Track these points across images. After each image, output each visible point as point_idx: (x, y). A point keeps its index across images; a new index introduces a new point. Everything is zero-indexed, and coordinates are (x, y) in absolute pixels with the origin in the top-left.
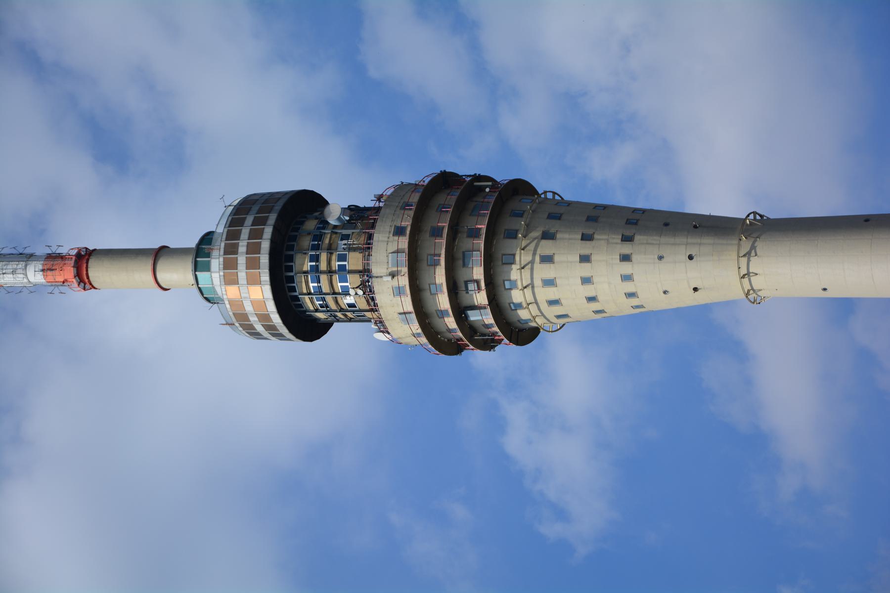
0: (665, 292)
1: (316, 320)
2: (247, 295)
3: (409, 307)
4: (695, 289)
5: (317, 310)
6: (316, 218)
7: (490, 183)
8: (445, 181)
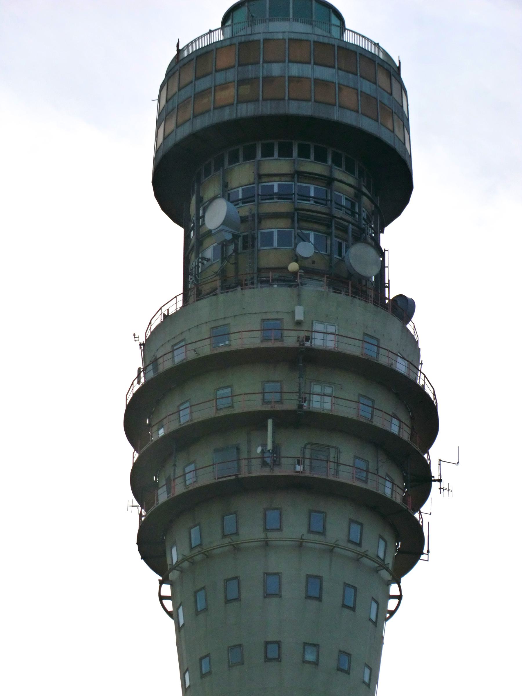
8: (425, 417)
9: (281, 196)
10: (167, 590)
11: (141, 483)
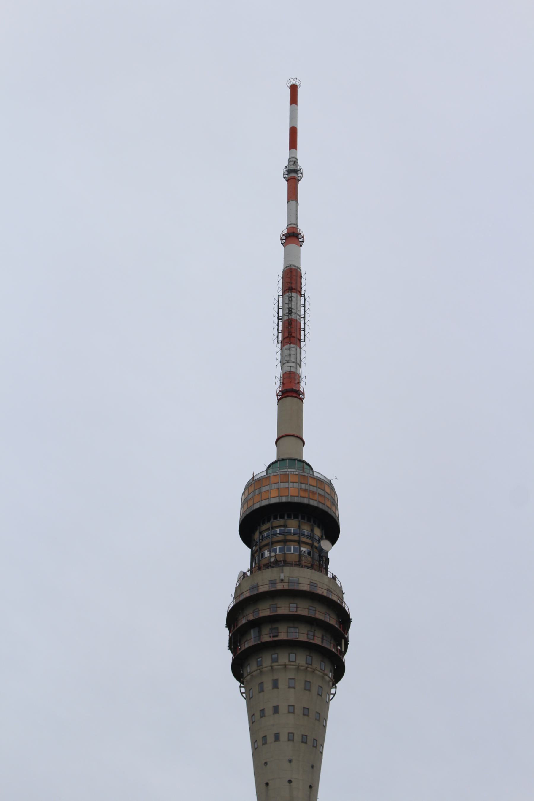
0: (266, 763)
1: (254, 533)
2: (273, 488)
3: (262, 589)
4: (267, 784)
5: (261, 533)
6: (322, 536)
7: (343, 650)
8: (345, 620)
9: (294, 534)
10: (243, 690)
11: (233, 645)
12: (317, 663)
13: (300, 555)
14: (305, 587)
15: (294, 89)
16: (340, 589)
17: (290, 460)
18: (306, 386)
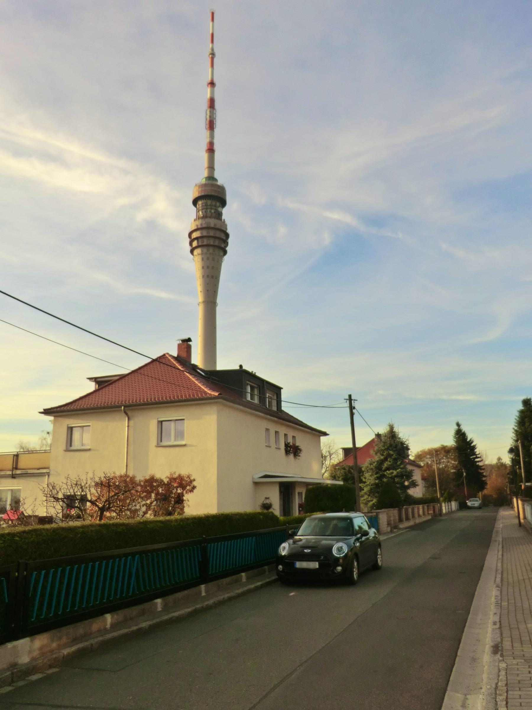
8: (227, 236)
12: (217, 251)
13: (212, 213)
14: (212, 226)
15: (213, 14)
16: (226, 225)
17: (211, 178)
18: (216, 147)
